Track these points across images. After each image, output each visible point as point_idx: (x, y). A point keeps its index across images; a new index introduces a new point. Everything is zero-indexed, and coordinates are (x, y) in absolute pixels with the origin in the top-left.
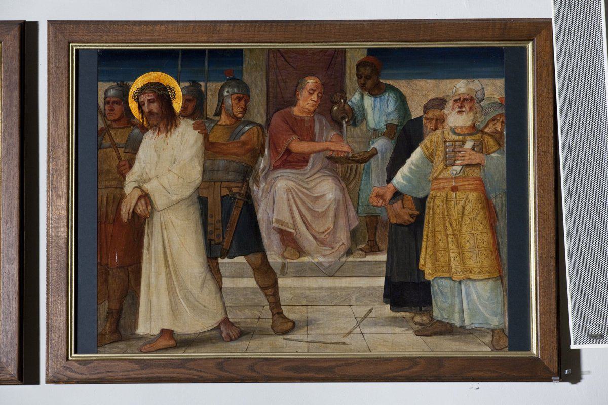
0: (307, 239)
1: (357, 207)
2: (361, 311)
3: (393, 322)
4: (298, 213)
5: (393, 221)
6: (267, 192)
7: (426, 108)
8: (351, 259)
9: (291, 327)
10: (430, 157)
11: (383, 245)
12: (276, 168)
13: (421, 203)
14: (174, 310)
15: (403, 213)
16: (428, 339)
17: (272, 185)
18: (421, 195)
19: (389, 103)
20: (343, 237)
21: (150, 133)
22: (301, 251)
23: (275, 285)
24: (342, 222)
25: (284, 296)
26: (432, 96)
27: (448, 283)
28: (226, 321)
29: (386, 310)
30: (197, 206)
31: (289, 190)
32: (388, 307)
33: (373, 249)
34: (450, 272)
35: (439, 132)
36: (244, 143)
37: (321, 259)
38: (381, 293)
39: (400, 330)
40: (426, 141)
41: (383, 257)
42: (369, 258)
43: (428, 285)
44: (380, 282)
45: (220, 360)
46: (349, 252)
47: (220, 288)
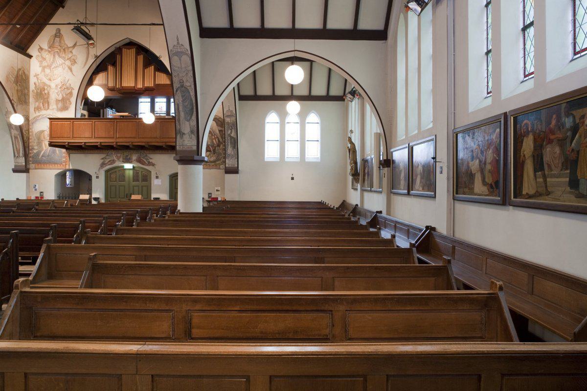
0: (553, 167)
1: (563, 155)
2: (563, 189)
3: (570, 193)
4: (89, 77)
5: (571, 159)
6: (545, 152)
7: (580, 119)
8: (562, 172)
9: (548, 193)
10: (580, 136)
11: (569, 167)
12: (547, 144)
13: (578, 152)
14: (529, 189)
15: (573, 156)
16: (578, 199)
17: (546, 150)
18: (578, 150)
19: (571, 119)
20: (560, 165)
21: (525, 138)
22: (551, 170)
23: (546, 180)
24: (560, 160)
25: (548, 184)
26: (582, 114)
27: (583, 180)
28: (537, 191)
29: (568, 189)
30: (532, 158)
31: (550, 151)
32: (569, 188)
33: (567, 169)
34: (118, 138)
35: (583, 127)
36: (541, 138)
37: (555, 172)
38: (567, 183)
39: (571, 195)
40: (580, 131)
41: (568, 171)
42: (566, 172)
43: (578, 181)
44: (568, 179)
45: (173, 234)
46: (561, 170)
47: (536, 180)
